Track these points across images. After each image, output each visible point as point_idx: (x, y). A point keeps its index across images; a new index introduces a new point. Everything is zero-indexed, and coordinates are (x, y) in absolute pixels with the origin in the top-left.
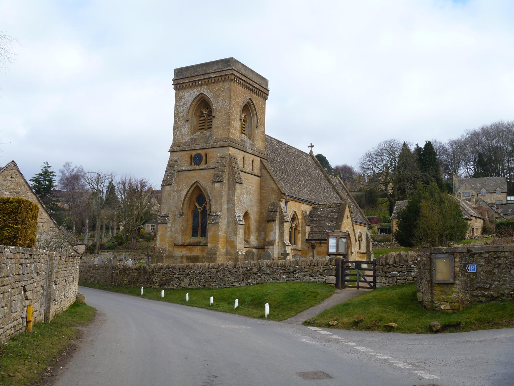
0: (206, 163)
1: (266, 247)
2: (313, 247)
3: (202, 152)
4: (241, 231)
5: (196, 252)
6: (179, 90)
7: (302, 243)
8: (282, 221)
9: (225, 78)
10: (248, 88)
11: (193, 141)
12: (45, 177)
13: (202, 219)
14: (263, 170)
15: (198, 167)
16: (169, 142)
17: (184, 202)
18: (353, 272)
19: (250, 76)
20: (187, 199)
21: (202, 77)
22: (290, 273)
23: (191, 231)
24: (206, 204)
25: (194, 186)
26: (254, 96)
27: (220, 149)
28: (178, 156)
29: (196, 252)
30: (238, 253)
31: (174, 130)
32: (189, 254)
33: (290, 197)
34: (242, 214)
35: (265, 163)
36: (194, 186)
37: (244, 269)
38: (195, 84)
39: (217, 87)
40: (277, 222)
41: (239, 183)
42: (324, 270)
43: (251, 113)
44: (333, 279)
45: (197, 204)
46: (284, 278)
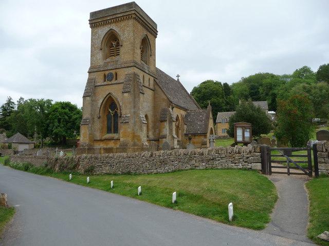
0: (116, 79)
1: (160, 139)
2: (190, 139)
3: (113, 72)
4: (145, 128)
5: (111, 145)
6: (94, 27)
7: (182, 136)
8: (171, 122)
9: (127, 17)
10: (145, 27)
11: (106, 64)
12: (9, 105)
13: (114, 120)
14: (156, 86)
15: (110, 83)
16: (88, 66)
17: (100, 107)
18: (279, 159)
19: (146, 18)
20: (102, 106)
21: (111, 17)
22: (209, 160)
23: (106, 130)
24: (117, 109)
25: (108, 97)
26: (149, 33)
27: (127, 69)
28: (94, 75)
29: (111, 145)
30: (143, 144)
31: (91, 57)
32: (105, 147)
33: (175, 104)
34: (144, 116)
35: (157, 81)
36: (108, 97)
37: (161, 158)
38: (106, 23)
39: (123, 24)
40: (168, 122)
41: (143, 93)
42: (248, 158)
43: (147, 46)
44: (259, 166)
45: (110, 110)
46: (203, 165)
